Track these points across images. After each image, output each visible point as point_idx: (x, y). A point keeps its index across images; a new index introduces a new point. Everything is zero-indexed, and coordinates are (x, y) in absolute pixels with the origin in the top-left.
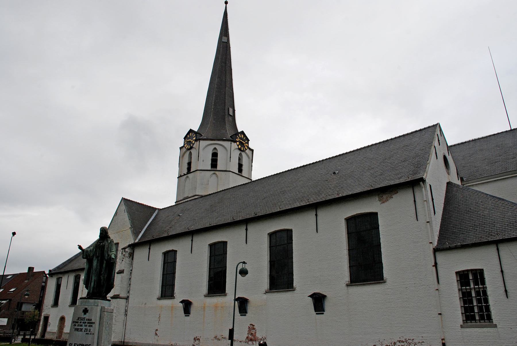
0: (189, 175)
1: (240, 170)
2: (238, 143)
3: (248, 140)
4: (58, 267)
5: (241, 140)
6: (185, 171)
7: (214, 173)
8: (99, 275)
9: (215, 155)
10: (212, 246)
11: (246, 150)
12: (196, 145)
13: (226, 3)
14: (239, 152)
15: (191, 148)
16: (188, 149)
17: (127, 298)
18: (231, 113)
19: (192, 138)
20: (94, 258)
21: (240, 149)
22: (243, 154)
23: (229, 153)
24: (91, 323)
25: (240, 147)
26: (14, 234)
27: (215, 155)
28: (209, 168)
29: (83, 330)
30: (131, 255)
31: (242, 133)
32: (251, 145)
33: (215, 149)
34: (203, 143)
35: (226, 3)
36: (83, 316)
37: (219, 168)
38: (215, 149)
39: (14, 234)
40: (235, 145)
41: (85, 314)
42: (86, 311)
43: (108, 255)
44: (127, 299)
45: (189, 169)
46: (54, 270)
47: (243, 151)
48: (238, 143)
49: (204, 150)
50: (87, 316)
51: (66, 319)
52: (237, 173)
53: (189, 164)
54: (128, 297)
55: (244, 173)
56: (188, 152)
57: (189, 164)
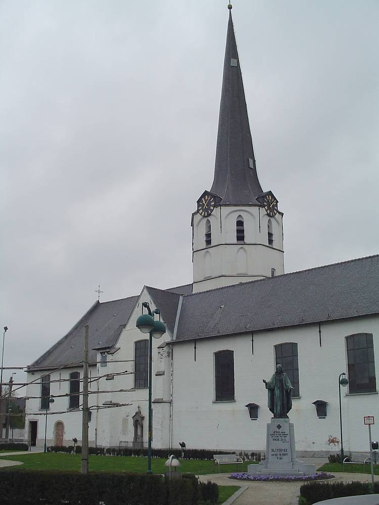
0: (209, 250)
1: (271, 241)
2: (266, 207)
3: (277, 202)
4: (37, 363)
5: (268, 202)
6: (203, 245)
7: (241, 248)
8: (283, 400)
9: (240, 223)
10: (278, 348)
11: (275, 214)
12: (216, 211)
13: (230, 7)
14: (267, 218)
15: (209, 215)
16: (204, 216)
17: (170, 402)
18: (251, 166)
19: (208, 203)
20: (276, 389)
21: (268, 215)
22: (272, 220)
23: (254, 218)
24: (285, 435)
25: (268, 211)
26: (6, 329)
27: (240, 223)
28: (235, 241)
29: (280, 440)
30: (170, 355)
31: (270, 193)
32: (280, 209)
33: (240, 216)
34: (225, 210)
35: (230, 7)
36: (278, 430)
37: (246, 240)
38: (240, 216)
39: (6, 329)
40: (263, 211)
41: (279, 429)
42: (279, 427)
43: (286, 386)
44: (170, 403)
45: (208, 242)
46: (33, 365)
47: (273, 216)
48: (266, 207)
49: (224, 220)
50: (280, 430)
51: (65, 424)
52: (268, 245)
53: (208, 236)
54: (172, 400)
55: (275, 245)
56: (205, 220)
57: (208, 236)
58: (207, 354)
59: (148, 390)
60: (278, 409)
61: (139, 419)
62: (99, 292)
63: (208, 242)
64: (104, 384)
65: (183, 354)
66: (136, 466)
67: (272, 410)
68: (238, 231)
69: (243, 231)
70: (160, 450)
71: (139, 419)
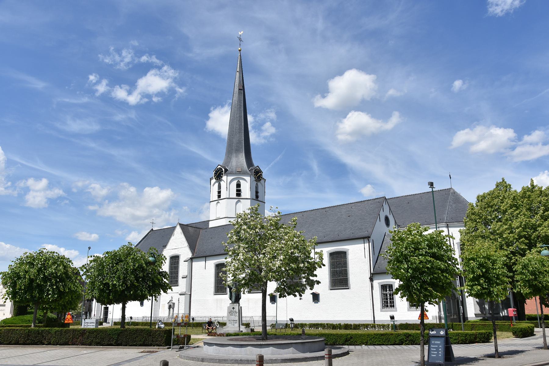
9: (238, 185)
24: (236, 313)
26: (89, 248)
28: (235, 196)
39: (89, 248)
45: (219, 196)
53: (219, 192)
57: (219, 192)
58: (211, 264)
59: (260, 295)
60: (234, 298)
61: (172, 304)
62: (153, 223)
63: (219, 196)
64: (13, 265)
65: (198, 265)
66: (151, 324)
67: (231, 299)
68: (237, 191)
69: (240, 191)
70: (133, 300)
71: (172, 304)
